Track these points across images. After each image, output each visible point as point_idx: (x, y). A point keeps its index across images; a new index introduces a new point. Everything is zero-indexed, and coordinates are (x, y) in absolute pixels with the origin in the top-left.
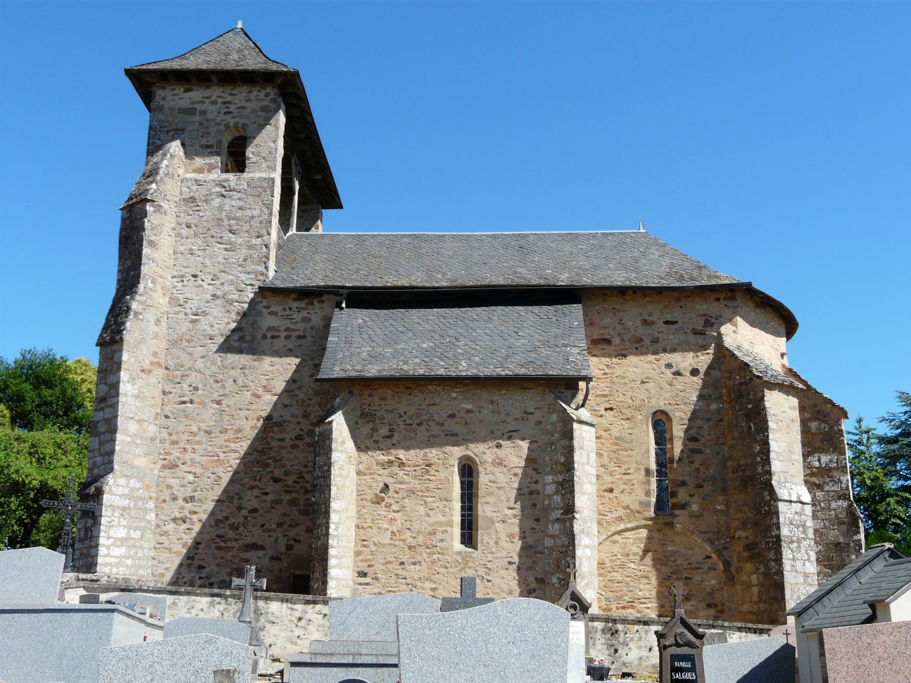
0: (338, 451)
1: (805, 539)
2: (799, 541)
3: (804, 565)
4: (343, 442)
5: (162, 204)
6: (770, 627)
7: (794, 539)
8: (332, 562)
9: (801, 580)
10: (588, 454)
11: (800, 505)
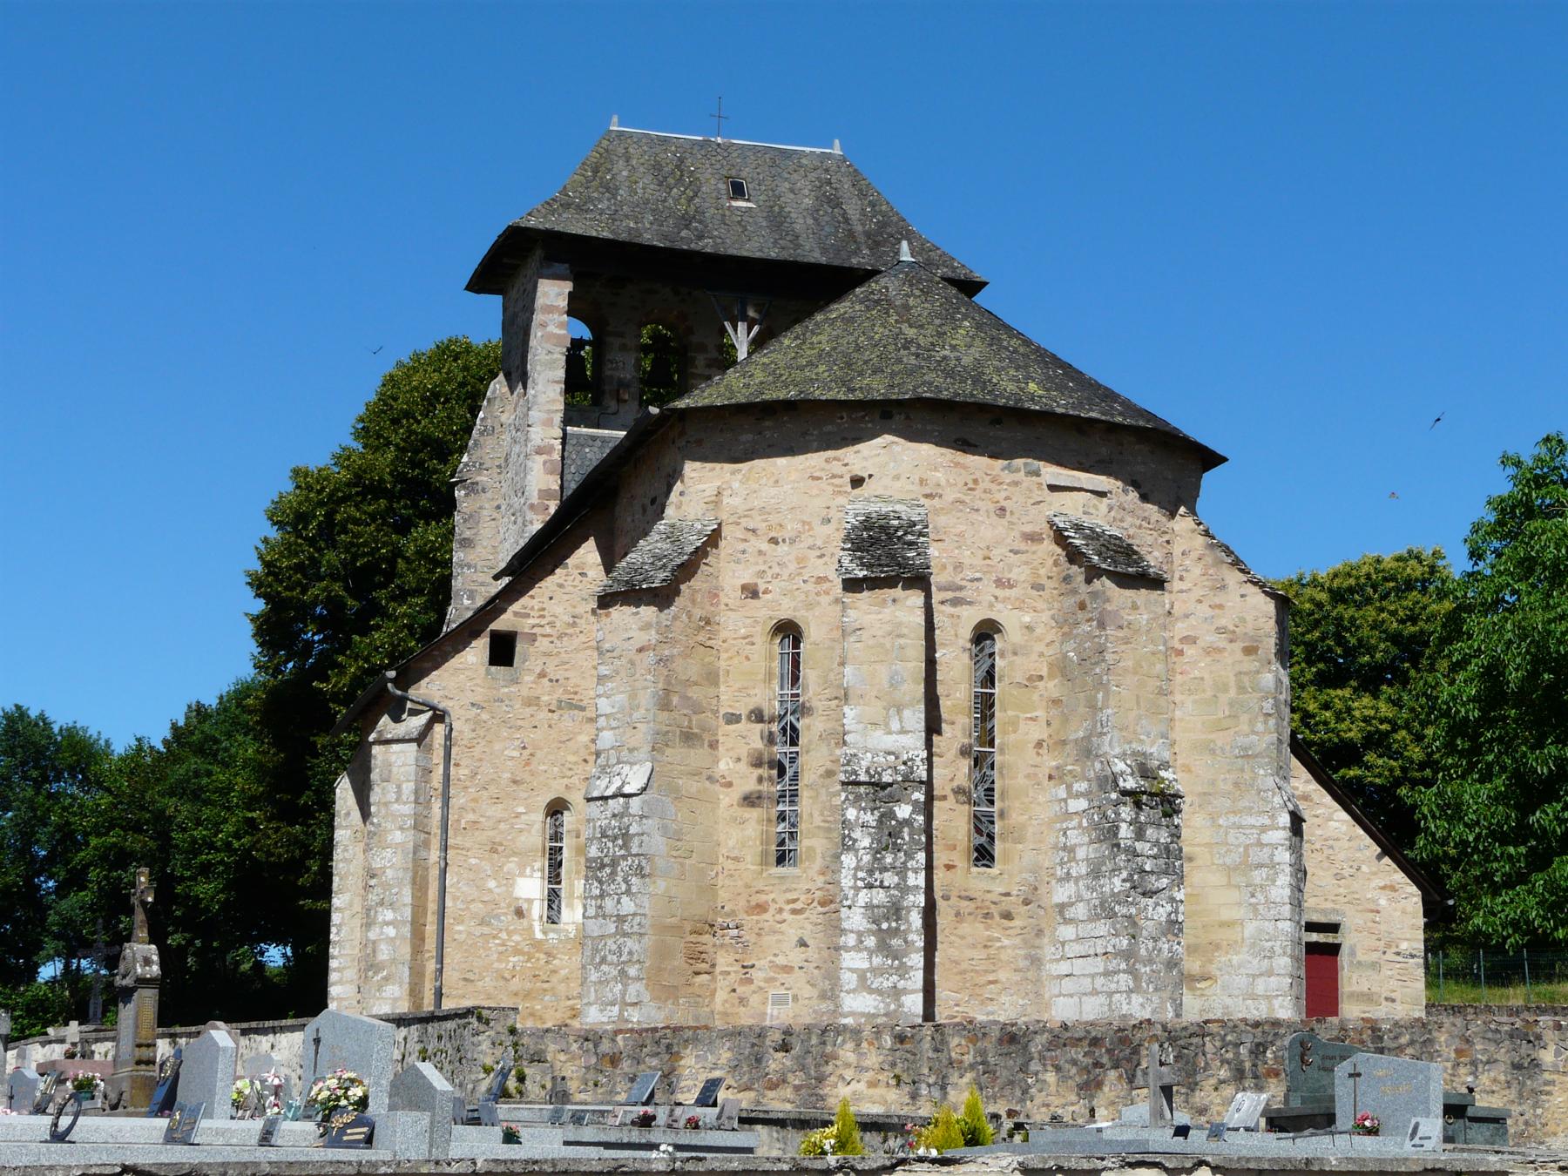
0: (341, 827)
1: (624, 857)
2: (614, 863)
3: (619, 902)
4: (348, 814)
5: (478, 479)
6: (201, 1027)
7: (606, 860)
8: (333, 977)
9: (612, 928)
10: (399, 787)
11: (621, 800)
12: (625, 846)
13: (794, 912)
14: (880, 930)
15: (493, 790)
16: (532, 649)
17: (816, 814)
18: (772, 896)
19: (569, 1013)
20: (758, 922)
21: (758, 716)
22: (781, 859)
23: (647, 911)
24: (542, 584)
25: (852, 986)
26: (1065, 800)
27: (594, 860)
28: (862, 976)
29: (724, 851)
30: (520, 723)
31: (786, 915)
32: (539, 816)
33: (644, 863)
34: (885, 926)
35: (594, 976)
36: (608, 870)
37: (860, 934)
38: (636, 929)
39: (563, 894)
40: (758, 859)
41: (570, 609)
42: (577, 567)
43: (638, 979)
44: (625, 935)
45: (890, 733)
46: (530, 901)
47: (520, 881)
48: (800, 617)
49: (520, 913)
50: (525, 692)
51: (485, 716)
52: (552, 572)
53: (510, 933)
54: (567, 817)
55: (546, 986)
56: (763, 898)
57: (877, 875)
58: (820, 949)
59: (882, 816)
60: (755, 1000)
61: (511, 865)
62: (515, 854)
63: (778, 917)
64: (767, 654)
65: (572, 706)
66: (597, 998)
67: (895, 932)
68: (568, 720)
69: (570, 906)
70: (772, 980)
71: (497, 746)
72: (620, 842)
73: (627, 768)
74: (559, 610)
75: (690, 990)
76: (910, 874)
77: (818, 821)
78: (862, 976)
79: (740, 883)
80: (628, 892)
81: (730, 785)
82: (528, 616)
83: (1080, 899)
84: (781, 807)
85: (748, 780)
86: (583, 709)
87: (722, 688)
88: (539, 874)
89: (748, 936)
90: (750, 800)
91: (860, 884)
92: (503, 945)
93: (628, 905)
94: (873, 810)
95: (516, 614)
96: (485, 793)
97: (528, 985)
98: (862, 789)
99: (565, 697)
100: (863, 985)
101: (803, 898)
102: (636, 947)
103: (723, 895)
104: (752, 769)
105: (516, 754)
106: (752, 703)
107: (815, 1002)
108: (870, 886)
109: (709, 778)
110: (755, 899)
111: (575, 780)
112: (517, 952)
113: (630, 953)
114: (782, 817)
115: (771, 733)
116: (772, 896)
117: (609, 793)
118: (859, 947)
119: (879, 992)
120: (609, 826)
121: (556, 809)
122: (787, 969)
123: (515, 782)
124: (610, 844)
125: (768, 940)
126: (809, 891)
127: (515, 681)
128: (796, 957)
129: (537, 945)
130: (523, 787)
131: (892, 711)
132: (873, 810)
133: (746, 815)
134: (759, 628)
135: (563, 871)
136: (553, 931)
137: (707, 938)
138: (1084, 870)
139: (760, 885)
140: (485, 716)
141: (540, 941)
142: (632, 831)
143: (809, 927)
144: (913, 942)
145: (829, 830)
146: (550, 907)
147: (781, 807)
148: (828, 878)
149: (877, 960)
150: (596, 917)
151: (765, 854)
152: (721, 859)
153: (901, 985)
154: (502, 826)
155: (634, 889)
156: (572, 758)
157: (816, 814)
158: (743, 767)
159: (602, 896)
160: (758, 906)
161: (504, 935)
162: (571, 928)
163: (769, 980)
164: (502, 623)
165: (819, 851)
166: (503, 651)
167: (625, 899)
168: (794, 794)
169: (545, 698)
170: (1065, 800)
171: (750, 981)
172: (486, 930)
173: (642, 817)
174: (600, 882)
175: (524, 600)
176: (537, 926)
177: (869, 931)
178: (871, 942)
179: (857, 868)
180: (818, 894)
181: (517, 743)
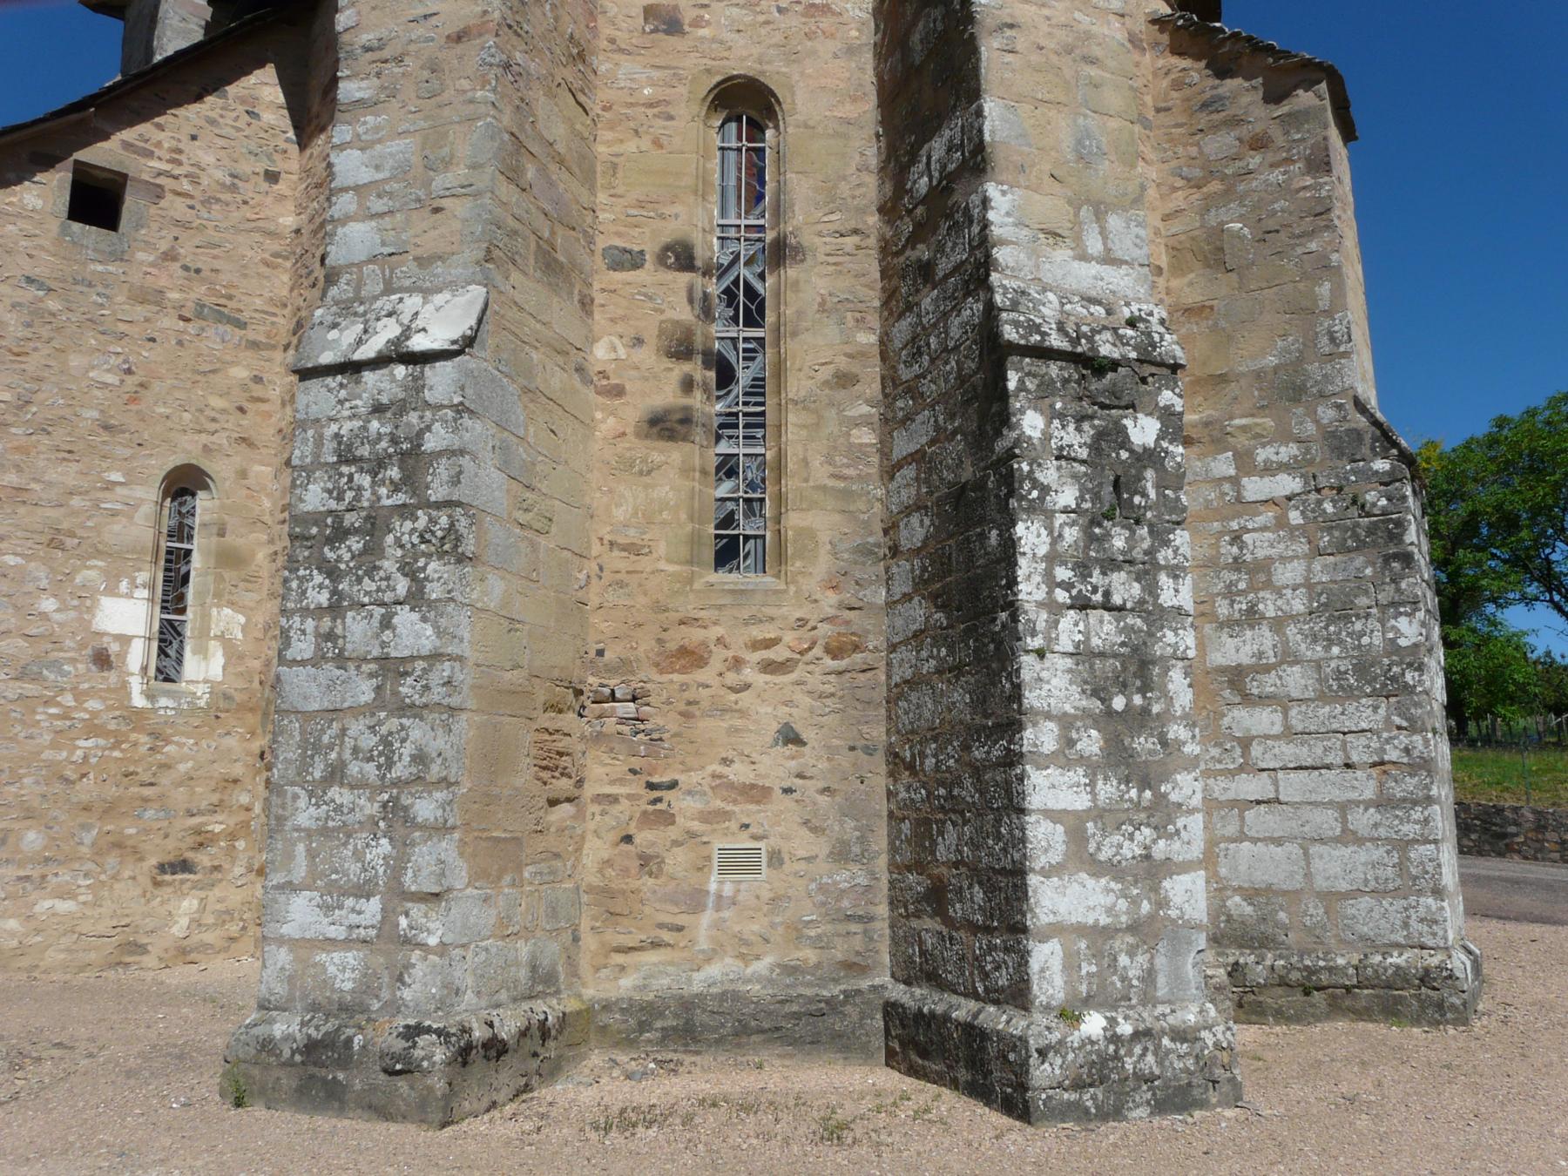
1: (405, 511)
2: (375, 525)
3: (386, 623)
7: (351, 519)
9: (364, 690)
11: (400, 371)
12: (410, 481)
13: (769, 667)
14: (1110, 713)
15: (60, 435)
16: (153, 210)
17: (816, 462)
18: (717, 631)
19: (190, 841)
20: (684, 687)
21: (681, 257)
22: (727, 554)
23: (465, 649)
24: (181, 112)
25: (1055, 857)
26: (1235, 481)
27: (317, 518)
28: (1074, 825)
29: (604, 531)
30: (122, 327)
31: (749, 674)
32: (149, 493)
33: (462, 525)
34: (1119, 703)
35: (306, 815)
36: (356, 543)
37: (1066, 722)
38: (437, 694)
39: (188, 632)
40: (684, 552)
41: (226, 162)
42: (243, 101)
43: (441, 829)
44: (405, 709)
45: (1084, 257)
46: (125, 640)
47: (106, 602)
48: (774, 73)
49: (102, 660)
50: (136, 278)
51: (53, 304)
52: (199, 98)
53: (80, 696)
54: (203, 503)
55: (147, 791)
56: (695, 635)
57: (1096, 577)
58: (831, 751)
59: (1100, 435)
60: (677, 861)
61: (90, 574)
62: (99, 553)
63: (731, 678)
64: (700, 143)
65: (222, 317)
66: (313, 874)
67: (1140, 719)
68: (214, 338)
69: (202, 651)
70: (725, 815)
71: (75, 361)
72: (394, 473)
73: (413, 302)
74: (208, 159)
75: (541, 843)
76: (1164, 579)
77: (820, 473)
78: (1074, 825)
79: (642, 600)
80: (416, 598)
81: (618, 391)
82: (149, 154)
83: (1289, 657)
84: (724, 448)
85: (662, 386)
86: (242, 325)
87: (602, 197)
88: (145, 593)
89: (661, 719)
90: (666, 426)
91: (1061, 596)
92: (65, 717)
93: (412, 632)
94: (1080, 419)
95: (127, 145)
96: (45, 440)
97: (112, 791)
98: (1054, 369)
99: (210, 300)
100: (1081, 858)
101: (789, 637)
102: (438, 743)
103: (602, 626)
104: (668, 363)
105: (111, 379)
106: (671, 231)
107: (822, 866)
108: (1082, 605)
109: (580, 370)
110: (678, 637)
111: (221, 439)
112: (93, 728)
113: (420, 758)
114: (728, 468)
115: (706, 296)
116: (717, 631)
117: (367, 352)
118: (1065, 756)
119: (1112, 869)
120: (362, 435)
121: (183, 484)
122: (756, 793)
123: (107, 428)
124: (366, 480)
125: (709, 727)
126: (802, 622)
127: (119, 257)
128: (775, 766)
129: (136, 718)
130: (120, 438)
131: (1086, 212)
132: (1080, 419)
133: (656, 457)
134: (682, 90)
135: (191, 592)
136: (168, 694)
137: (569, 720)
138: (1298, 605)
139: (688, 607)
140: (53, 304)
141: (140, 713)
142: (431, 443)
143: (807, 701)
144: (1180, 744)
145: (846, 494)
146: (162, 652)
147: (724, 448)
148: (847, 597)
149: (1107, 790)
150: (317, 660)
151: (694, 540)
152: (596, 549)
153: (1160, 849)
154: (76, 502)
155: (434, 591)
156: (217, 402)
157: (816, 462)
158: (647, 356)
159: (335, 609)
160: (683, 651)
161: (68, 700)
162: (200, 690)
163: (709, 817)
164: (104, 153)
165: (824, 537)
166: (97, 202)
167: (405, 618)
168: (757, 422)
169: (174, 295)
170: (1235, 481)
171: (668, 818)
172: (30, 688)
173: (460, 409)
174: (333, 573)
175: (144, 128)
176: (136, 685)
177: (1086, 713)
178: (1091, 742)
179: (1053, 558)
180: (825, 629)
181: (113, 360)
